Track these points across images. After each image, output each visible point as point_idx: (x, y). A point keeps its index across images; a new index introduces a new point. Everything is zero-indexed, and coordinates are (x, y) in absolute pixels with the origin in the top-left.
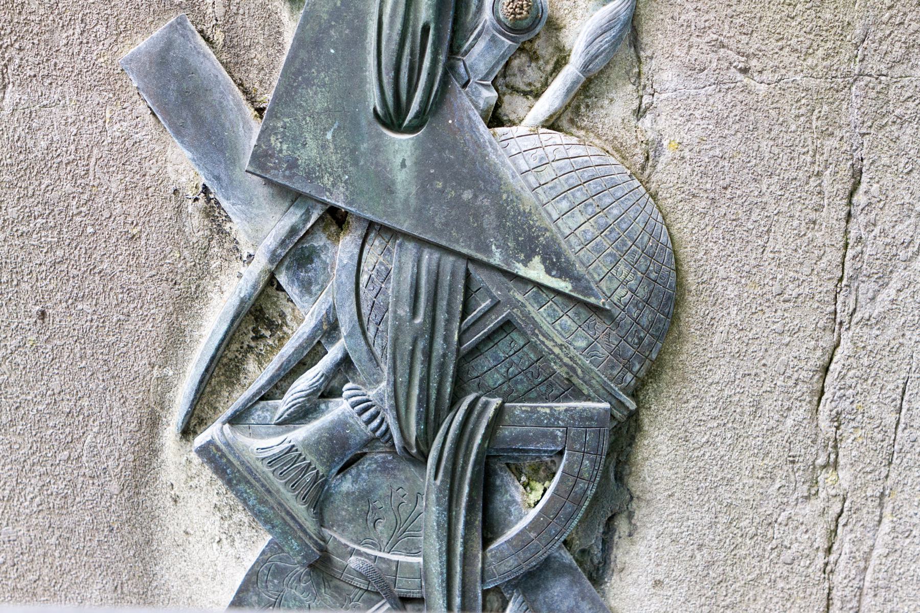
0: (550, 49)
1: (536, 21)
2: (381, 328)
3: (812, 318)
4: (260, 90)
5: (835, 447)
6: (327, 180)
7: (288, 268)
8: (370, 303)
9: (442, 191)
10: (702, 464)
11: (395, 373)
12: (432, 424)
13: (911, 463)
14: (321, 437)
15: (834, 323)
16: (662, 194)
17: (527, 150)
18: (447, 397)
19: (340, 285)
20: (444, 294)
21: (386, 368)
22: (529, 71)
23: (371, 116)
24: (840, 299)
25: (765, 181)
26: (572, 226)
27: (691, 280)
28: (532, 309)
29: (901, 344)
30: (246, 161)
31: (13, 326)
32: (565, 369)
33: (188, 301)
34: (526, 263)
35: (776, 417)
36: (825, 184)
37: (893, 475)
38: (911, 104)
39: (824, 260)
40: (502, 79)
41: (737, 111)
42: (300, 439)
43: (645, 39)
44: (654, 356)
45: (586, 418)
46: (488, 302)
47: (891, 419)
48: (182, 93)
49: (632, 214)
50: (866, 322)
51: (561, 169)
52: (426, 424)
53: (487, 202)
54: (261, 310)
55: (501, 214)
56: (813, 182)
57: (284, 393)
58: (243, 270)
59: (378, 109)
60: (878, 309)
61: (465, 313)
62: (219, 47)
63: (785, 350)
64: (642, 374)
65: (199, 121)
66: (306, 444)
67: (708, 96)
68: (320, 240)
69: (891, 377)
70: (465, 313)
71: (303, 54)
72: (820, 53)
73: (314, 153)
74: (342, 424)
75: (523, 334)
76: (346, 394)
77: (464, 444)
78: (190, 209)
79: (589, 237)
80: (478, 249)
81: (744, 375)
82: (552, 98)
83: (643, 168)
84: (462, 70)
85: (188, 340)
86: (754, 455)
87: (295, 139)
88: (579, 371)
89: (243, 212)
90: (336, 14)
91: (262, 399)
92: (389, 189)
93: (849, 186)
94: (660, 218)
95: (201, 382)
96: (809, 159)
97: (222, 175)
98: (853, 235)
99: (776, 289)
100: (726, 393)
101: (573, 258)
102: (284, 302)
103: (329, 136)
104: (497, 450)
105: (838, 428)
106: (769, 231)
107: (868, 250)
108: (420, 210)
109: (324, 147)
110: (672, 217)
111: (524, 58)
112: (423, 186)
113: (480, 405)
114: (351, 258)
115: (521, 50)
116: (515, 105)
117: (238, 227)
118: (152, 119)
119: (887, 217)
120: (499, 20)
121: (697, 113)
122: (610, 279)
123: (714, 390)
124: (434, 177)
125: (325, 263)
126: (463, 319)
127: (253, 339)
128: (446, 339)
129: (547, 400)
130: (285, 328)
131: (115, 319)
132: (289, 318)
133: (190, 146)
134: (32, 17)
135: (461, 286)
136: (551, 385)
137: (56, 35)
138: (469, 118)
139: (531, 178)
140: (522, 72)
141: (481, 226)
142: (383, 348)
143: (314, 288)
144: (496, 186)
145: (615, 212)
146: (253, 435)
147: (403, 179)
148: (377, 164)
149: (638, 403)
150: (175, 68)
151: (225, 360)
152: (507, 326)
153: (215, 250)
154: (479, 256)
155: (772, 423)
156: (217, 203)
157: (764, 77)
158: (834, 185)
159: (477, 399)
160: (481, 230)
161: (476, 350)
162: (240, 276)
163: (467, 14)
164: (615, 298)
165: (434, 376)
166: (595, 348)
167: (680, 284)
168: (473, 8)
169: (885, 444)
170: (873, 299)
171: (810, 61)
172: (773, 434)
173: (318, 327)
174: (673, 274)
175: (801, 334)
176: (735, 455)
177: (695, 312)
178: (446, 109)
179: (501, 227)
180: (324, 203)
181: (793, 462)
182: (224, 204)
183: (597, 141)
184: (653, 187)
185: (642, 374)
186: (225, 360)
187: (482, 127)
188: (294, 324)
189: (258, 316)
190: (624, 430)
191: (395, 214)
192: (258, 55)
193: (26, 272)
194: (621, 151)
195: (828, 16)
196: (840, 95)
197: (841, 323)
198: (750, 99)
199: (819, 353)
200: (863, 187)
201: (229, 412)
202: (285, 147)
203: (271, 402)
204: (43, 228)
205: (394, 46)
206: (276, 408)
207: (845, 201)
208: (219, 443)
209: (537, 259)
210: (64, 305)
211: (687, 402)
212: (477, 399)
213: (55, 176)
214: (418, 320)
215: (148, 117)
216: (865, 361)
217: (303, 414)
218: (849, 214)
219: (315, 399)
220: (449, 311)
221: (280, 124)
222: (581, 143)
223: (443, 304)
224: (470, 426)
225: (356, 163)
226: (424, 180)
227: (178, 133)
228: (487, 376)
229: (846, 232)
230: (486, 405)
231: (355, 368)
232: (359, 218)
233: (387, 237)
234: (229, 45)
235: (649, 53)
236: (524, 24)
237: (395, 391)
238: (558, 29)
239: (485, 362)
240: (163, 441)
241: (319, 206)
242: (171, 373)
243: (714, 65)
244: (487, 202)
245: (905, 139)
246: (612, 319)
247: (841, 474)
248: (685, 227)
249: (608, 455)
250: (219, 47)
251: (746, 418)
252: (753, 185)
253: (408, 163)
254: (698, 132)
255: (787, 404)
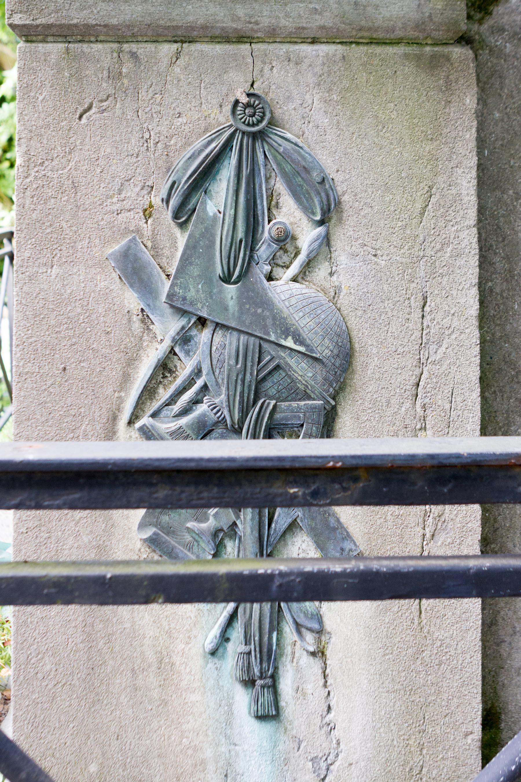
0: (293, 248)
1: (287, 237)
2: (222, 370)
3: (410, 361)
4: (167, 267)
5: (424, 420)
6: (199, 305)
7: (179, 345)
8: (217, 359)
9: (249, 309)
10: (365, 430)
11: (228, 390)
12: (245, 413)
13: (458, 426)
14: (194, 422)
15: (420, 363)
16: (342, 309)
17: (284, 291)
18: (252, 400)
19: (203, 351)
20: (250, 354)
21: (224, 389)
22: (284, 257)
23: (218, 278)
24: (422, 352)
25: (387, 302)
26: (304, 323)
27: (357, 346)
28: (288, 359)
29: (450, 372)
30: (163, 298)
31: (50, 375)
32: (303, 386)
33: (131, 362)
34: (285, 339)
35: (397, 407)
36: (412, 303)
37: (450, 432)
38: (445, 268)
39: (414, 336)
40: (273, 261)
41: (373, 272)
42: (184, 423)
43: (333, 243)
44: (342, 380)
45: (313, 408)
46: (269, 357)
47: (448, 406)
48: (133, 268)
49: (330, 318)
50: (434, 363)
51: (299, 299)
52: (242, 413)
53: (268, 314)
54: (166, 365)
55: (274, 318)
56: (407, 302)
57: (176, 403)
58: (158, 346)
59: (221, 275)
60: (438, 357)
61: (259, 362)
62: (150, 248)
63: (399, 376)
64: (337, 388)
65: (141, 280)
66: (187, 426)
67: (360, 266)
68: (194, 332)
69: (446, 387)
70: (259, 362)
71: (188, 252)
72: (406, 247)
73: (193, 294)
74: (204, 415)
75: (285, 371)
76: (205, 401)
77: (259, 422)
78: (134, 320)
79: (312, 327)
80: (264, 334)
81: (382, 388)
82: (294, 269)
83: (334, 298)
84: (256, 258)
85: (132, 379)
86: (389, 425)
87: (185, 288)
88: (310, 387)
89: (160, 320)
90: (202, 235)
91: (166, 405)
92: (226, 309)
93: (422, 303)
94: (342, 319)
95: (139, 398)
96: (404, 292)
97: (151, 304)
98: (425, 325)
99: (394, 349)
100: (375, 396)
101: (305, 337)
102: (177, 360)
103: (200, 286)
104: (274, 425)
105: (425, 411)
106: (389, 324)
107: (432, 331)
108: (239, 318)
109: (198, 291)
110: (347, 319)
111: (282, 252)
112: (240, 307)
113: (266, 404)
114: (208, 339)
115: (281, 248)
116: (278, 272)
117: (157, 328)
118: (119, 280)
119: (439, 316)
120: (271, 237)
121: (356, 274)
122: (322, 346)
123: (369, 395)
124: (245, 303)
125: (196, 342)
126: (258, 365)
127: (162, 378)
128: (251, 374)
129: (296, 401)
130: (177, 373)
131: (98, 370)
132: (178, 368)
133: (137, 292)
134: (66, 236)
135: (257, 350)
136: (297, 394)
137: (77, 244)
138: (260, 278)
139: (287, 303)
140: (281, 258)
141: (265, 324)
142: (223, 379)
143: (191, 354)
144: (272, 307)
145: (323, 317)
146: (163, 422)
147: (232, 304)
148: (221, 298)
149: (336, 402)
150: (131, 258)
151: (149, 388)
152: (278, 367)
153: (145, 337)
154: (265, 337)
155: (396, 410)
156: (148, 316)
157: (383, 258)
158: (416, 303)
159: (265, 401)
160: (265, 326)
161: (264, 379)
162: (157, 349)
163: (257, 234)
164: (324, 354)
165: (246, 390)
166: (316, 377)
167: (352, 348)
168: (260, 232)
169: (446, 418)
170: (436, 352)
171: (402, 251)
172: (396, 415)
173: (193, 371)
174: (349, 343)
175: (406, 369)
176: (380, 425)
177: (359, 361)
178: (250, 274)
179: (274, 324)
180: (196, 315)
181: (406, 428)
182: (151, 316)
183: (314, 287)
184: (338, 306)
185: (337, 388)
186: (149, 388)
187: (265, 281)
188: (181, 371)
189: (164, 368)
190: (330, 415)
191: (228, 319)
192: (166, 252)
193: (58, 349)
194: (324, 291)
195: (408, 232)
196: (416, 265)
197: (423, 364)
198: (378, 267)
199: (414, 377)
200: (428, 304)
201: (151, 412)
202: (181, 291)
203: (170, 407)
204: (67, 329)
205: (228, 248)
206: (173, 409)
207: (421, 310)
208: (148, 425)
209: (290, 338)
210: (75, 364)
211: (357, 401)
212: (265, 401)
213: (73, 305)
214: (239, 366)
215: (118, 280)
216: (434, 380)
217: (185, 412)
218: (423, 316)
219: (191, 404)
220: (252, 362)
221: (179, 282)
222: (307, 287)
223: (249, 358)
224: (262, 414)
225: (211, 298)
226: (241, 305)
227: (132, 286)
228: (269, 391)
229: (422, 323)
230: (269, 403)
231: (209, 390)
232: (212, 322)
233: (224, 329)
234: (154, 248)
235: (334, 249)
236: (282, 238)
237: (228, 398)
238: (296, 239)
239: (268, 384)
240: (118, 427)
241: (195, 317)
242: (123, 395)
243: (362, 253)
244: (268, 314)
245: (444, 283)
246: (323, 363)
247: (428, 432)
248: (353, 323)
249: (323, 427)
250: (150, 248)
251: (384, 408)
252: (381, 304)
253: (234, 297)
254: (357, 282)
255: (402, 401)
